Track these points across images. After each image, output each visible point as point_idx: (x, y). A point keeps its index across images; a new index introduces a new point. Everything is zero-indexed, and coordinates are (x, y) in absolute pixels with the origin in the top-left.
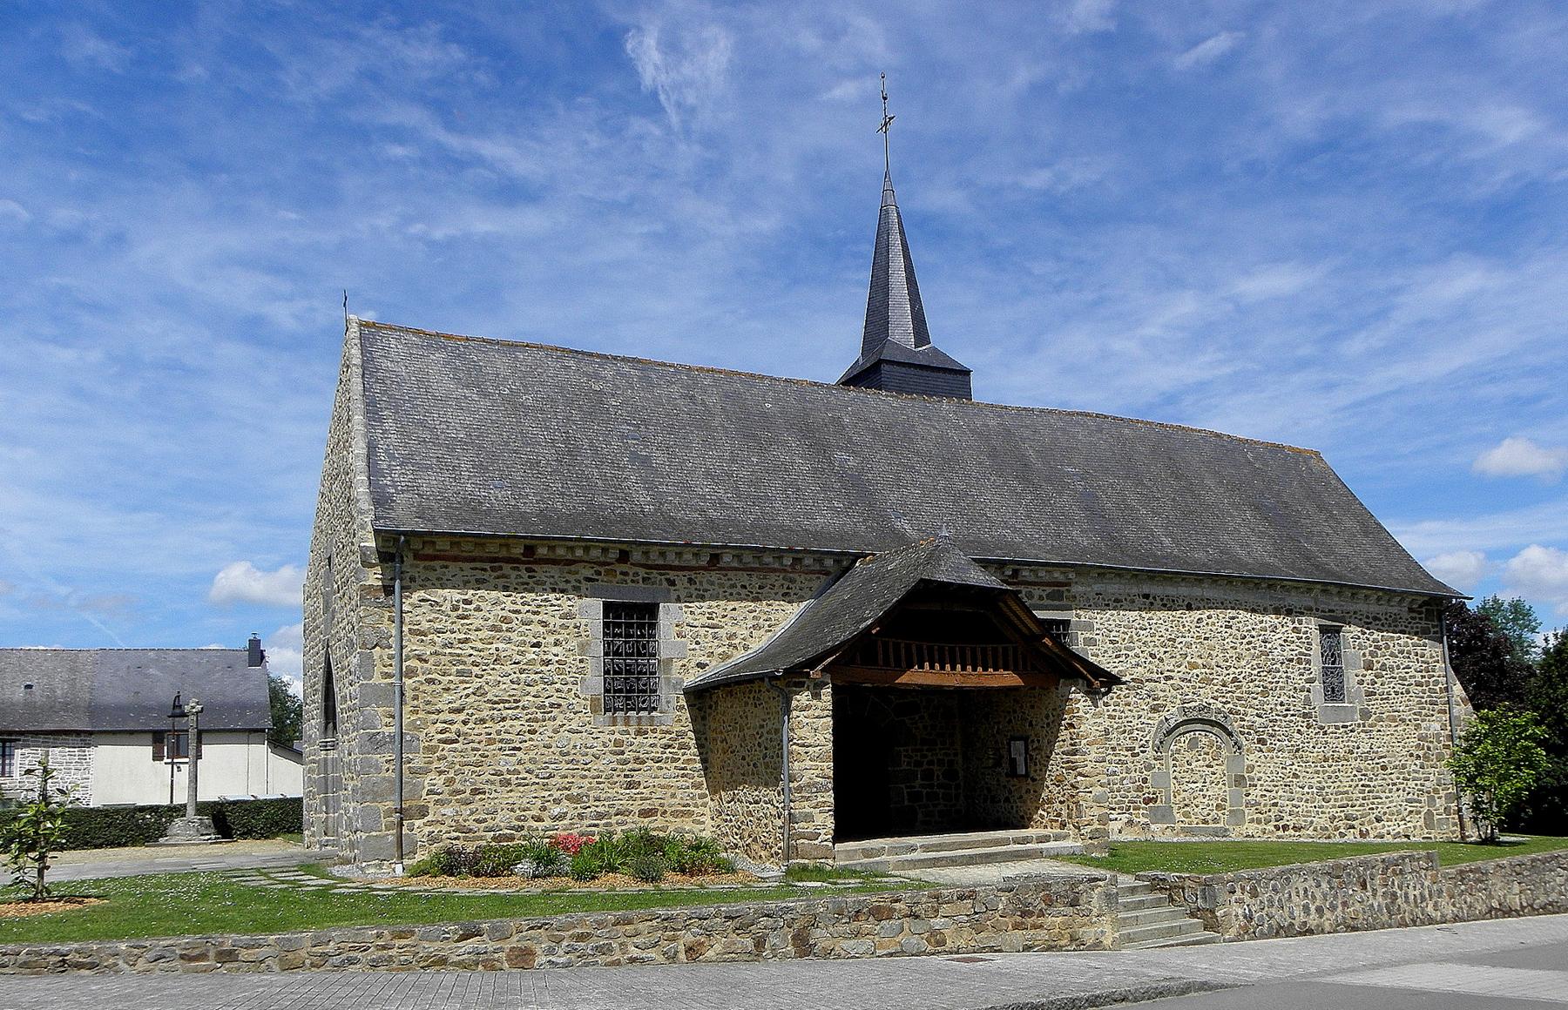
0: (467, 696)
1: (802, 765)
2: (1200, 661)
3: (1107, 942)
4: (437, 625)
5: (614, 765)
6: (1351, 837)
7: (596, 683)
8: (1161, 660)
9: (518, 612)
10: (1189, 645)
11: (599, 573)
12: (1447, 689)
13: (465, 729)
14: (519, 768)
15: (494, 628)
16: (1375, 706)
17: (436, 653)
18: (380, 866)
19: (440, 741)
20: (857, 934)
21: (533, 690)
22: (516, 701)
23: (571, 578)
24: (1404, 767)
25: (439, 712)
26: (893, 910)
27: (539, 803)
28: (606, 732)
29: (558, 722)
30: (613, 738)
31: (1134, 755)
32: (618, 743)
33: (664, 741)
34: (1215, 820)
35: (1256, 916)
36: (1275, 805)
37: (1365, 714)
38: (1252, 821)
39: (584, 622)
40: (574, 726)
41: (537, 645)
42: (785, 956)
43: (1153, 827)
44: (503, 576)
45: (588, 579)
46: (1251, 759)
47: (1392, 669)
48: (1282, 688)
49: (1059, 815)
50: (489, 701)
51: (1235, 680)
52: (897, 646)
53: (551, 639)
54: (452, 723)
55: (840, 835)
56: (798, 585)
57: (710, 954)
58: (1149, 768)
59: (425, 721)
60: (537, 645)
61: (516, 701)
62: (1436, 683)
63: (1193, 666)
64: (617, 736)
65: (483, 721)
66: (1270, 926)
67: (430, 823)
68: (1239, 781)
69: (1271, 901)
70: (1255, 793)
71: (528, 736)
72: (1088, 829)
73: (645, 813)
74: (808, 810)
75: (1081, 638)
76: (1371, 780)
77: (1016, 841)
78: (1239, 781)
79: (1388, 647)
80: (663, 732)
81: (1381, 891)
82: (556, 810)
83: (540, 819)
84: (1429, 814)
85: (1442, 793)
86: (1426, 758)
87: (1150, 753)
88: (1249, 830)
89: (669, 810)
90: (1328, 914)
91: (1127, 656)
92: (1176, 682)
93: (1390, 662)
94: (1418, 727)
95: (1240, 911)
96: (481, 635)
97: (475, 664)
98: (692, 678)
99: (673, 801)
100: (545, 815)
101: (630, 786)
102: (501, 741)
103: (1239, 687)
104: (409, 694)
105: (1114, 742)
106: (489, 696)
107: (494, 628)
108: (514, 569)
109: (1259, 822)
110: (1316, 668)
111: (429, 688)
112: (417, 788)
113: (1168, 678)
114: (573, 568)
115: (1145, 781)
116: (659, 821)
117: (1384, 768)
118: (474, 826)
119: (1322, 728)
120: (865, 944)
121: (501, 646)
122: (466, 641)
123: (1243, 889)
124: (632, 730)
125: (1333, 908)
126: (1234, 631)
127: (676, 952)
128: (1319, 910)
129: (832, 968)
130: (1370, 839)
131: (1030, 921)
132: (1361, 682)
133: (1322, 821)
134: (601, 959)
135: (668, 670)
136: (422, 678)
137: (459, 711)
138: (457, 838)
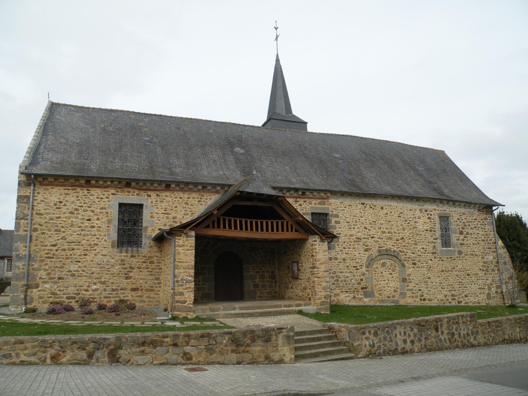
0: (58, 240)
1: (179, 271)
2: (387, 231)
3: (287, 359)
4: (47, 211)
6: (454, 303)
7: (114, 236)
8: (369, 230)
9: (82, 206)
10: (382, 224)
12: (495, 243)
13: (57, 253)
14: (79, 269)
15: (71, 213)
16: (464, 249)
17: (46, 222)
18: (17, 308)
19: (46, 257)
20: (143, 352)
21: (86, 238)
22: (79, 242)
23: (106, 193)
24: (477, 274)
25: (46, 246)
26: (164, 342)
27: (87, 284)
28: (119, 255)
29: (97, 251)
30: (120, 258)
31: (357, 269)
32: (122, 260)
33: (143, 260)
34: (393, 297)
35: (376, 345)
36: (420, 290)
37: (460, 253)
38: (410, 297)
39: (110, 211)
40: (104, 253)
41: (89, 220)
42: (103, 362)
43: (365, 300)
44: (77, 192)
45: (113, 194)
46: (409, 271)
47: (471, 234)
48: (423, 242)
49: (309, 295)
50: (68, 242)
51: (402, 238)
53: (95, 218)
54: (51, 250)
55: (196, 301)
56: (205, 197)
57: (64, 360)
58: (364, 274)
59: (40, 250)
60: (89, 220)
61: (79, 242)
62: (491, 240)
63: (384, 232)
65: (64, 250)
66: (384, 351)
67: (40, 291)
68: (404, 280)
69: (385, 338)
70: (411, 285)
71: (83, 257)
72: (320, 301)
74: (181, 290)
75: (333, 221)
76: (463, 280)
77: (285, 306)
78: (404, 280)
79: (469, 225)
80: (142, 256)
81: (446, 332)
82: (94, 287)
83: (87, 291)
84: (489, 294)
85: (494, 285)
86: (487, 271)
87: (364, 269)
88: (409, 301)
89: (144, 289)
90: (416, 344)
91: (354, 228)
92: (376, 239)
93: (470, 231)
94: (483, 258)
95: (367, 343)
96: (65, 215)
97: (62, 227)
99: (146, 285)
100: (89, 289)
101: (127, 278)
102: (72, 258)
103: (403, 241)
104: (34, 238)
105: (348, 264)
106: (68, 240)
107: (71, 213)
108: (81, 190)
109: (413, 297)
110: (438, 233)
111: (43, 236)
112: (35, 276)
113: (372, 237)
114: (107, 190)
115: (362, 280)
117: (468, 275)
118: (58, 293)
119: (441, 258)
120: (148, 358)
121: (74, 220)
122: (59, 217)
123: (370, 332)
124: (129, 255)
125: (420, 340)
126: (402, 218)
127: (45, 359)
128: (412, 342)
129: (131, 372)
130: (463, 304)
131: (241, 349)
132: (458, 240)
133: (441, 297)
134: (5, 361)
135: (146, 231)
136: (40, 232)
137: (55, 245)
138: (50, 297)
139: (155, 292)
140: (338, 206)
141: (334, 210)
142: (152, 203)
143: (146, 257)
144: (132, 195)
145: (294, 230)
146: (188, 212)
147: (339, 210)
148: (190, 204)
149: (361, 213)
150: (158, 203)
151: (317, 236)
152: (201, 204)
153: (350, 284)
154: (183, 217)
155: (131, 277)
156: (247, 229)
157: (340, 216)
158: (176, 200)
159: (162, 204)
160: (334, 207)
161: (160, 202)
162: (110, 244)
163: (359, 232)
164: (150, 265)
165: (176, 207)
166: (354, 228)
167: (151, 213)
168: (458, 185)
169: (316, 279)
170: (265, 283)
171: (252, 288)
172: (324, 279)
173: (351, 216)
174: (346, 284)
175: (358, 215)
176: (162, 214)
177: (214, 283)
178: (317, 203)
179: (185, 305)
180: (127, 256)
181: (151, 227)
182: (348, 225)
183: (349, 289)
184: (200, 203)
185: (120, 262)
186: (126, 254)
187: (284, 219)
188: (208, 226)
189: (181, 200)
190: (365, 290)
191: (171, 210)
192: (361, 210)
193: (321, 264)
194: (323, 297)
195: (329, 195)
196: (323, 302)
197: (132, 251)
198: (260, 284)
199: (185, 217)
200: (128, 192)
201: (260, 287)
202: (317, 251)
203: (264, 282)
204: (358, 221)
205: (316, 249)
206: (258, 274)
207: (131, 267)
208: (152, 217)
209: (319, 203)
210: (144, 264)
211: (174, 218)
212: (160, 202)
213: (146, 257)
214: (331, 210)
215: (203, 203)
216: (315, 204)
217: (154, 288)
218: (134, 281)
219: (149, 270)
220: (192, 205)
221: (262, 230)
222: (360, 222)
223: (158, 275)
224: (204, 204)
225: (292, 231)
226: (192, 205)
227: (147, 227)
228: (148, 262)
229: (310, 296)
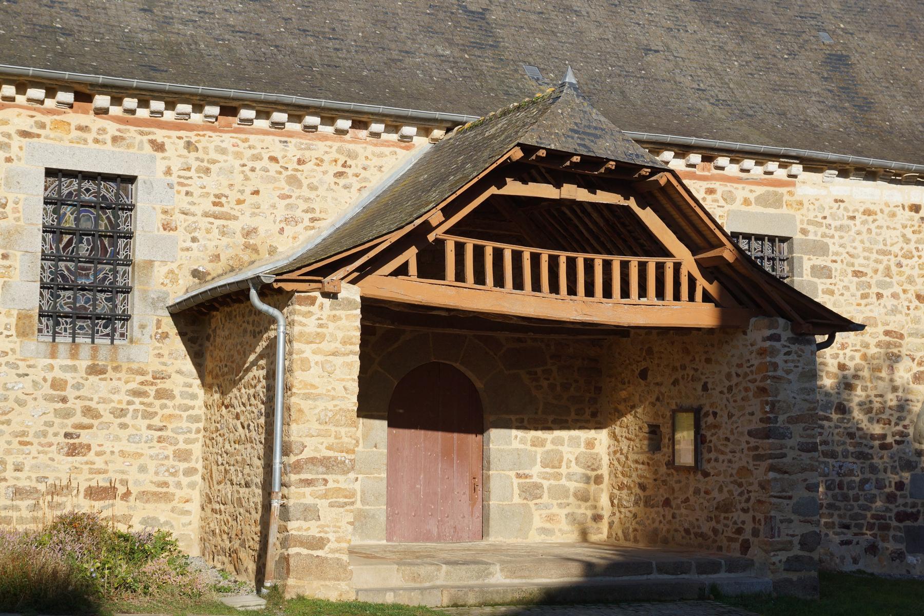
5: (50, 417)
11: (43, 126)
32: (57, 384)
33: (133, 385)
43: (910, 559)
45: (25, 134)
52: (479, 252)
56: (361, 161)
64: (58, 374)
73: (93, 493)
74: (309, 500)
98: (181, 290)
99: (141, 477)
101: (73, 451)
116: (119, 507)
124: (83, 364)
139: (174, 503)
140: (826, 213)
141: (811, 228)
142: (168, 172)
143: (142, 373)
144: (96, 141)
145: (699, 295)
146: (298, 213)
147: (829, 226)
148: (305, 182)
149: (908, 241)
150: (192, 173)
151: (781, 321)
152: (346, 187)
153: (856, 499)
154: (282, 231)
155: (89, 447)
156: (537, 287)
157: (832, 248)
158: (258, 165)
159: (206, 180)
160: (811, 216)
161: (198, 170)
162: (13, 321)
163: (894, 311)
164: (158, 403)
165: (256, 192)
166: (879, 296)
167: (165, 212)
168: (717, 102)
169: (771, 475)
170: (563, 481)
171: (517, 500)
172: (800, 476)
173: (870, 250)
174: (846, 498)
175: (895, 249)
176: (206, 215)
177: (384, 475)
178: (752, 197)
179: (320, 553)
180: (74, 369)
181: (164, 262)
182: (859, 286)
183: (852, 517)
184: (342, 181)
185: (47, 389)
186: (70, 362)
187: (667, 254)
188: (402, 270)
189: (273, 167)
190: (908, 523)
191: (239, 202)
192: (908, 232)
193: (792, 420)
194: (796, 540)
195: (797, 169)
196: (797, 558)
197: (95, 350)
198: (546, 484)
199: (289, 230)
200: (80, 128)
201: (545, 496)
202: (780, 373)
203: (558, 476)
204: (894, 269)
205: (775, 366)
206: (540, 450)
207: (88, 411)
208: (166, 227)
209: (762, 201)
210: (137, 400)
211: (249, 233)
212: (198, 170)
213: (142, 373)
214: (799, 226)
215: (351, 180)
216: (747, 202)
217: (171, 489)
218: (99, 463)
219: (156, 422)
220: (312, 188)
221: (590, 292)
222: (900, 274)
223: (187, 441)
224: (356, 186)
225: (692, 298)
226: (312, 188)
227: (151, 263)
228: (152, 390)
229: (747, 535)
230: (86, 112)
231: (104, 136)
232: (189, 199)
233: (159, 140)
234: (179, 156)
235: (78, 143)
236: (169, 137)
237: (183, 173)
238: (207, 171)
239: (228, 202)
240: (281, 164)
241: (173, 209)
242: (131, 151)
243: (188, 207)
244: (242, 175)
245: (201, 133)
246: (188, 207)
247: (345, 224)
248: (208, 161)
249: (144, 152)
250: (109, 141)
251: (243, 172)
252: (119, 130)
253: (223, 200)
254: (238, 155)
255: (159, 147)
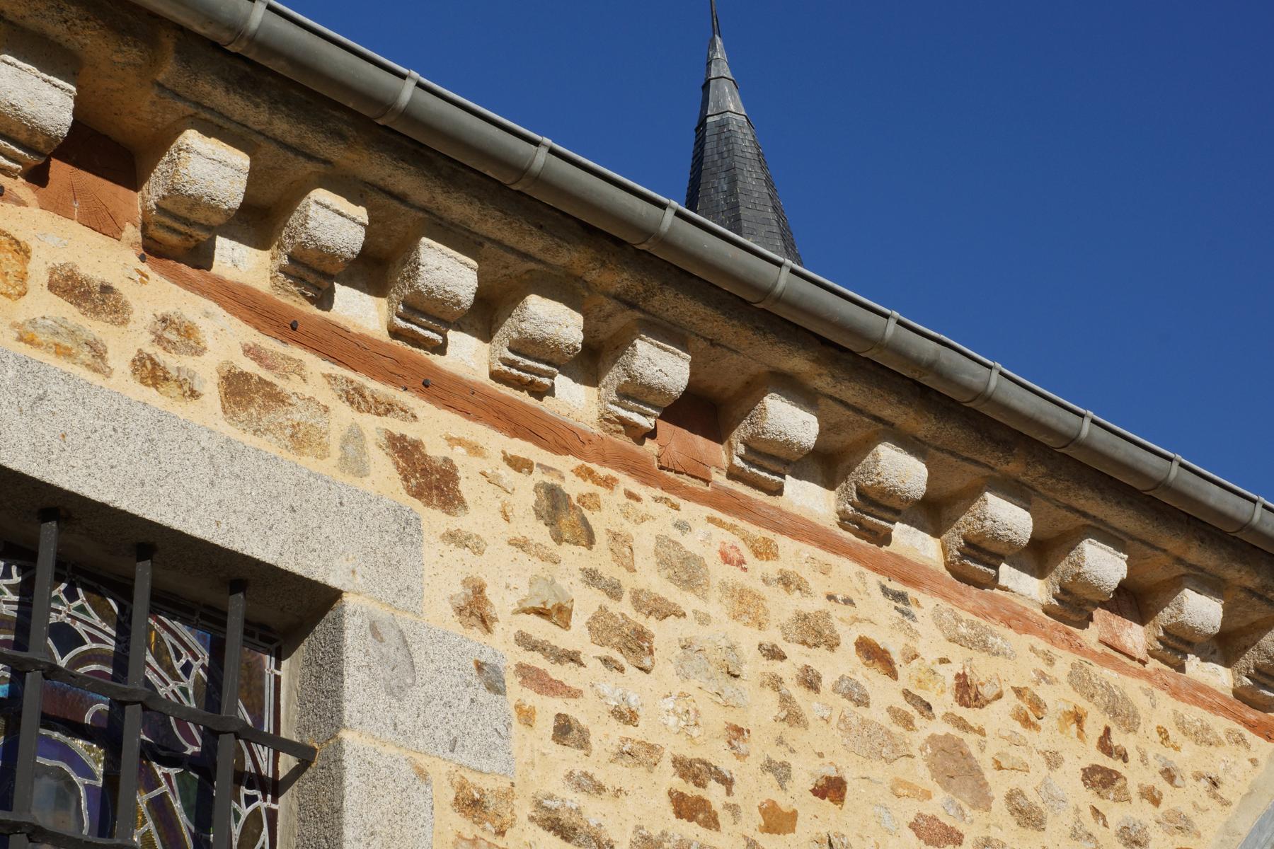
142: (475, 609)
159: (632, 686)
165: (832, 789)
200: (69, 286)
230: (103, 222)
231: (188, 362)
232: (569, 758)
233: (435, 450)
234: (521, 544)
235: (63, 352)
236: (475, 450)
237: (539, 629)
238: (638, 644)
239: (734, 809)
240: (904, 682)
241: (507, 796)
242: (308, 462)
243: (574, 798)
244: (771, 698)
245: (603, 471)
246: (574, 798)
247: (246, 321)
248: (636, 599)
249: (365, 485)
250: (212, 392)
251: (775, 683)
252: (252, 352)
253: (714, 793)
254: (746, 605)
255: (435, 483)
